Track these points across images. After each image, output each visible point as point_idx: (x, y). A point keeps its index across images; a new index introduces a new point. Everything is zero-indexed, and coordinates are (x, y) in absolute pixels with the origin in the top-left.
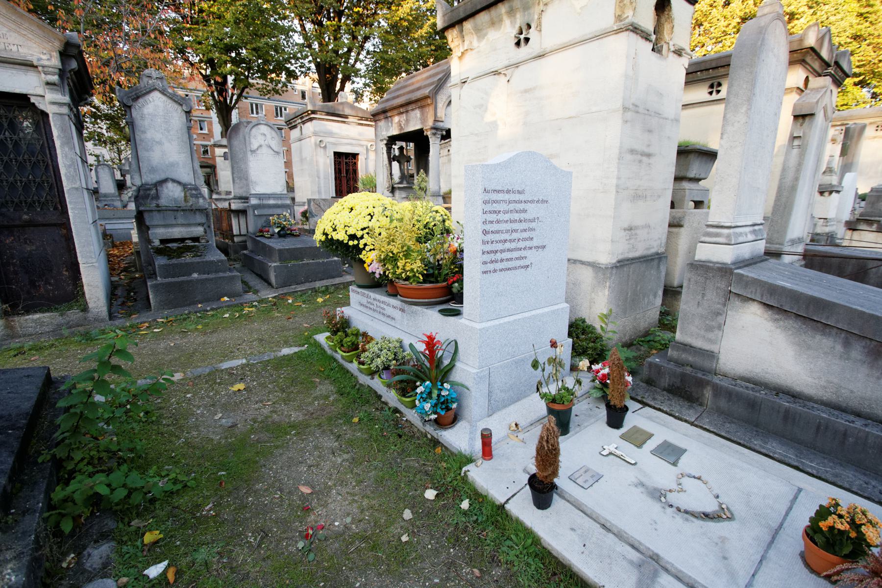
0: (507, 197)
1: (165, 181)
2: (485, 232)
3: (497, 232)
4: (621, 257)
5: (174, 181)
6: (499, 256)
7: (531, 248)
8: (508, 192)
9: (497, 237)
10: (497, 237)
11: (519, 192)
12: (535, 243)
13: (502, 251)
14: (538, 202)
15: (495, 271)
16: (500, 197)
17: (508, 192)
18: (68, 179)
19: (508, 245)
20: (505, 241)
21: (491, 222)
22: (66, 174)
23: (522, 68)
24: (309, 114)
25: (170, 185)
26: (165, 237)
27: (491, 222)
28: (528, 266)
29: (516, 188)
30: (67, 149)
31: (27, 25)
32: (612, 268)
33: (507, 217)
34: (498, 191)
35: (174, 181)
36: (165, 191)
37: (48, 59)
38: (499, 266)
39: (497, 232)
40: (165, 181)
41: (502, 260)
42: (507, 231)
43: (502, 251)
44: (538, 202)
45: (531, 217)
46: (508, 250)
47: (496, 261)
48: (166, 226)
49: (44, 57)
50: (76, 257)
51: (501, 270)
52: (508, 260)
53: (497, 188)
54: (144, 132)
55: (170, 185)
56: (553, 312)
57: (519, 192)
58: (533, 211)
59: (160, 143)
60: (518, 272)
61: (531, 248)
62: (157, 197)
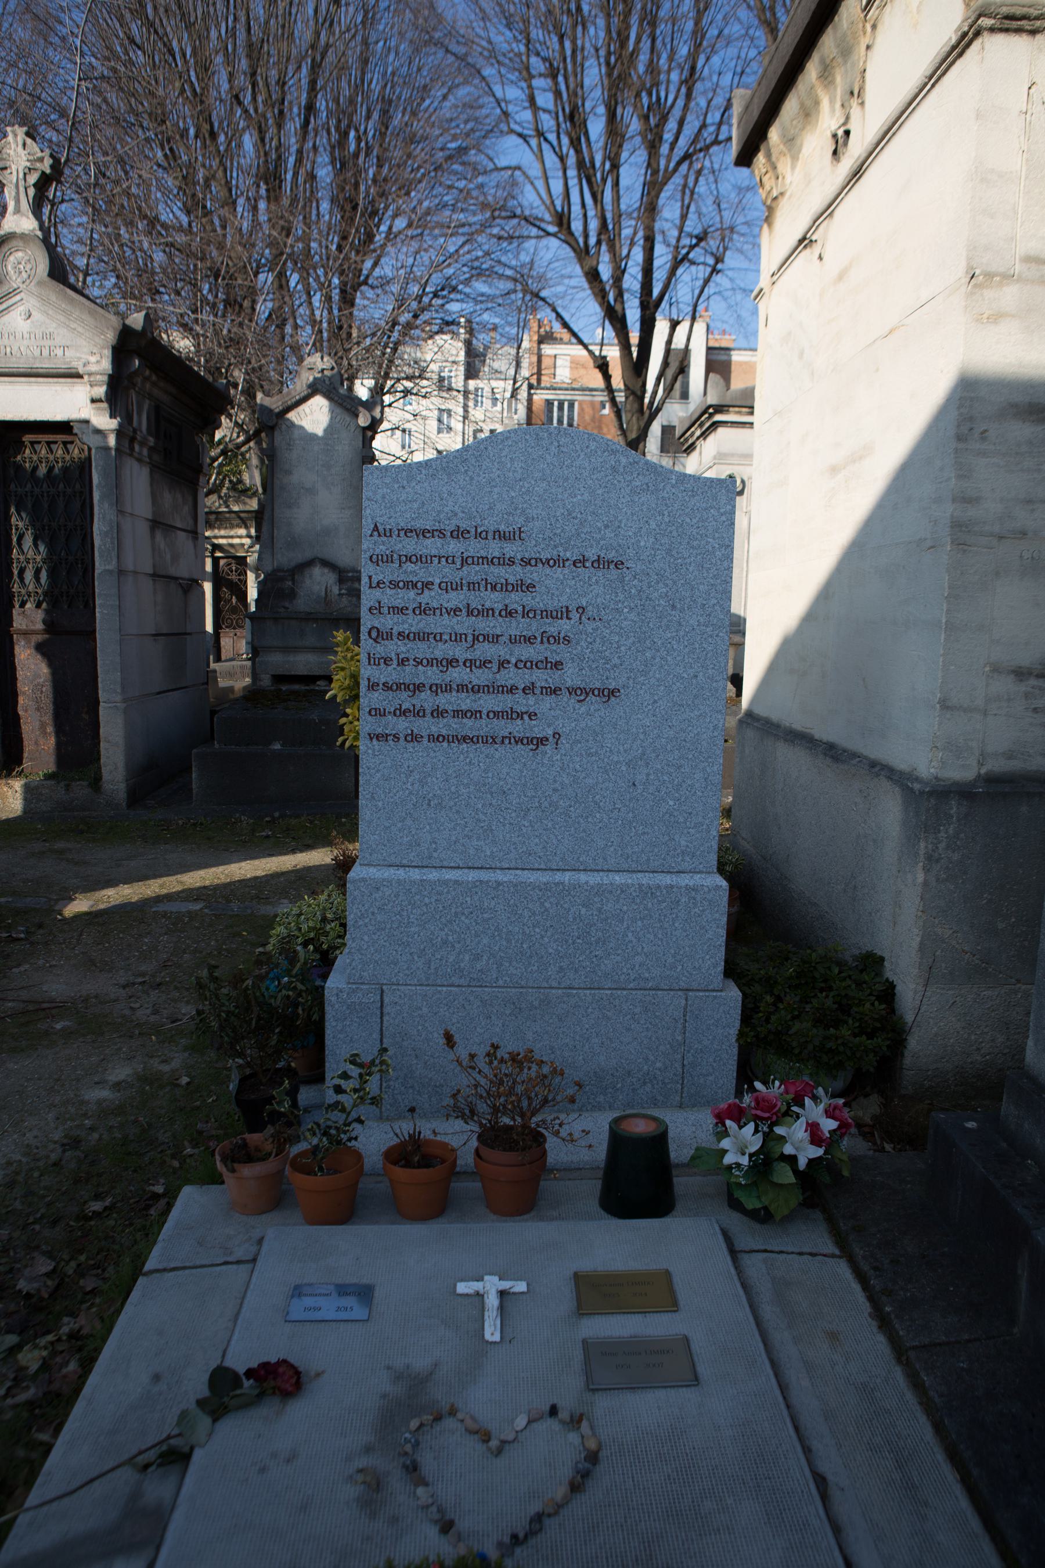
0: (454, 547)
1: (310, 563)
2: (456, 640)
3: (421, 636)
4: (997, 766)
5: (326, 563)
6: (426, 700)
7: (555, 691)
8: (459, 534)
9: (421, 650)
10: (421, 650)
11: (502, 536)
12: (570, 676)
13: (436, 689)
14: (581, 562)
15: (413, 738)
16: (431, 546)
17: (459, 534)
18: (101, 556)
19: (458, 675)
20: (452, 662)
21: (401, 610)
22: (100, 548)
23: (841, 211)
24: (711, 415)
25: (317, 571)
26: (280, 672)
27: (401, 610)
28: (542, 741)
29: (490, 524)
30: (106, 505)
31: (77, 313)
32: (931, 794)
33: (454, 599)
34: (424, 533)
35: (326, 563)
36: (308, 582)
37: (98, 362)
38: (427, 726)
39: (421, 636)
40: (310, 563)
41: (438, 713)
42: (458, 638)
43: (436, 689)
44: (581, 562)
45: (552, 604)
46: (462, 688)
47: (420, 713)
48: (286, 650)
49: (93, 359)
50: (97, 693)
51: (432, 738)
52: (458, 713)
53: (419, 525)
54: (289, 472)
55: (317, 571)
56: (647, 892)
57: (502, 536)
58: (555, 587)
59: (311, 491)
60: (500, 752)
61: (555, 691)
62: (292, 595)
